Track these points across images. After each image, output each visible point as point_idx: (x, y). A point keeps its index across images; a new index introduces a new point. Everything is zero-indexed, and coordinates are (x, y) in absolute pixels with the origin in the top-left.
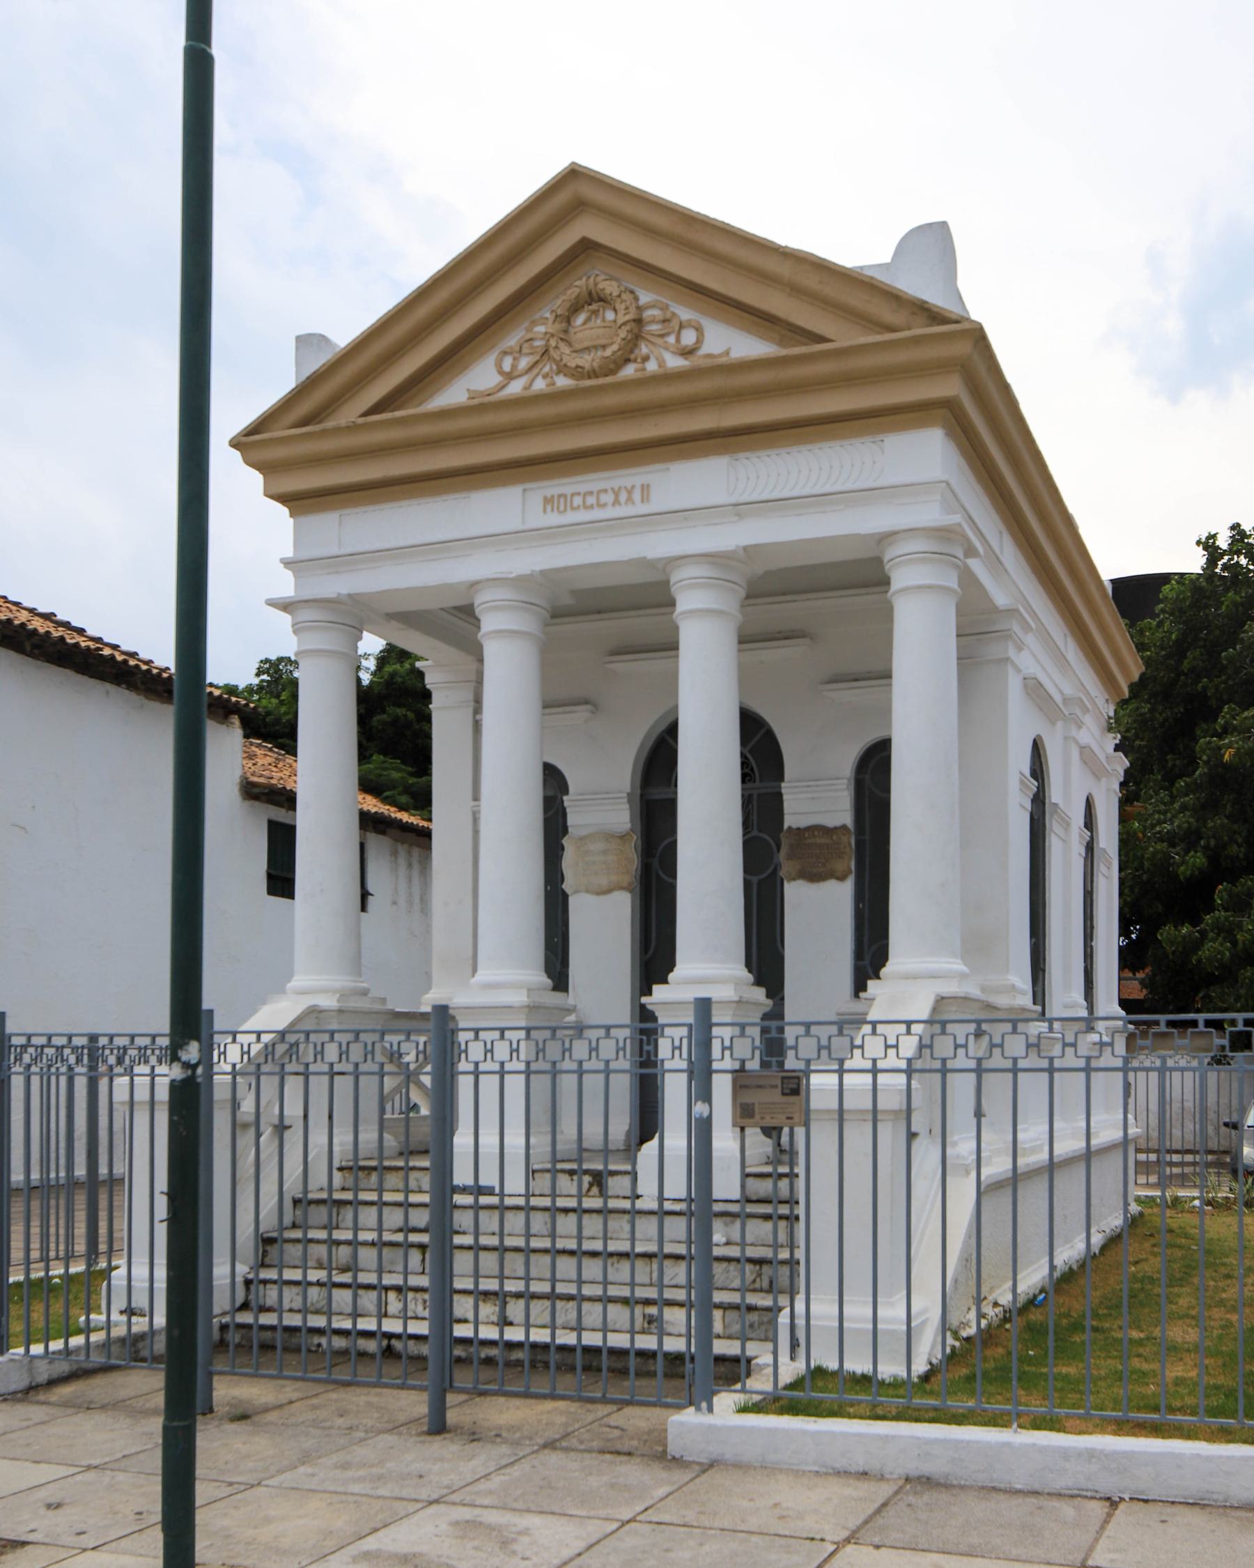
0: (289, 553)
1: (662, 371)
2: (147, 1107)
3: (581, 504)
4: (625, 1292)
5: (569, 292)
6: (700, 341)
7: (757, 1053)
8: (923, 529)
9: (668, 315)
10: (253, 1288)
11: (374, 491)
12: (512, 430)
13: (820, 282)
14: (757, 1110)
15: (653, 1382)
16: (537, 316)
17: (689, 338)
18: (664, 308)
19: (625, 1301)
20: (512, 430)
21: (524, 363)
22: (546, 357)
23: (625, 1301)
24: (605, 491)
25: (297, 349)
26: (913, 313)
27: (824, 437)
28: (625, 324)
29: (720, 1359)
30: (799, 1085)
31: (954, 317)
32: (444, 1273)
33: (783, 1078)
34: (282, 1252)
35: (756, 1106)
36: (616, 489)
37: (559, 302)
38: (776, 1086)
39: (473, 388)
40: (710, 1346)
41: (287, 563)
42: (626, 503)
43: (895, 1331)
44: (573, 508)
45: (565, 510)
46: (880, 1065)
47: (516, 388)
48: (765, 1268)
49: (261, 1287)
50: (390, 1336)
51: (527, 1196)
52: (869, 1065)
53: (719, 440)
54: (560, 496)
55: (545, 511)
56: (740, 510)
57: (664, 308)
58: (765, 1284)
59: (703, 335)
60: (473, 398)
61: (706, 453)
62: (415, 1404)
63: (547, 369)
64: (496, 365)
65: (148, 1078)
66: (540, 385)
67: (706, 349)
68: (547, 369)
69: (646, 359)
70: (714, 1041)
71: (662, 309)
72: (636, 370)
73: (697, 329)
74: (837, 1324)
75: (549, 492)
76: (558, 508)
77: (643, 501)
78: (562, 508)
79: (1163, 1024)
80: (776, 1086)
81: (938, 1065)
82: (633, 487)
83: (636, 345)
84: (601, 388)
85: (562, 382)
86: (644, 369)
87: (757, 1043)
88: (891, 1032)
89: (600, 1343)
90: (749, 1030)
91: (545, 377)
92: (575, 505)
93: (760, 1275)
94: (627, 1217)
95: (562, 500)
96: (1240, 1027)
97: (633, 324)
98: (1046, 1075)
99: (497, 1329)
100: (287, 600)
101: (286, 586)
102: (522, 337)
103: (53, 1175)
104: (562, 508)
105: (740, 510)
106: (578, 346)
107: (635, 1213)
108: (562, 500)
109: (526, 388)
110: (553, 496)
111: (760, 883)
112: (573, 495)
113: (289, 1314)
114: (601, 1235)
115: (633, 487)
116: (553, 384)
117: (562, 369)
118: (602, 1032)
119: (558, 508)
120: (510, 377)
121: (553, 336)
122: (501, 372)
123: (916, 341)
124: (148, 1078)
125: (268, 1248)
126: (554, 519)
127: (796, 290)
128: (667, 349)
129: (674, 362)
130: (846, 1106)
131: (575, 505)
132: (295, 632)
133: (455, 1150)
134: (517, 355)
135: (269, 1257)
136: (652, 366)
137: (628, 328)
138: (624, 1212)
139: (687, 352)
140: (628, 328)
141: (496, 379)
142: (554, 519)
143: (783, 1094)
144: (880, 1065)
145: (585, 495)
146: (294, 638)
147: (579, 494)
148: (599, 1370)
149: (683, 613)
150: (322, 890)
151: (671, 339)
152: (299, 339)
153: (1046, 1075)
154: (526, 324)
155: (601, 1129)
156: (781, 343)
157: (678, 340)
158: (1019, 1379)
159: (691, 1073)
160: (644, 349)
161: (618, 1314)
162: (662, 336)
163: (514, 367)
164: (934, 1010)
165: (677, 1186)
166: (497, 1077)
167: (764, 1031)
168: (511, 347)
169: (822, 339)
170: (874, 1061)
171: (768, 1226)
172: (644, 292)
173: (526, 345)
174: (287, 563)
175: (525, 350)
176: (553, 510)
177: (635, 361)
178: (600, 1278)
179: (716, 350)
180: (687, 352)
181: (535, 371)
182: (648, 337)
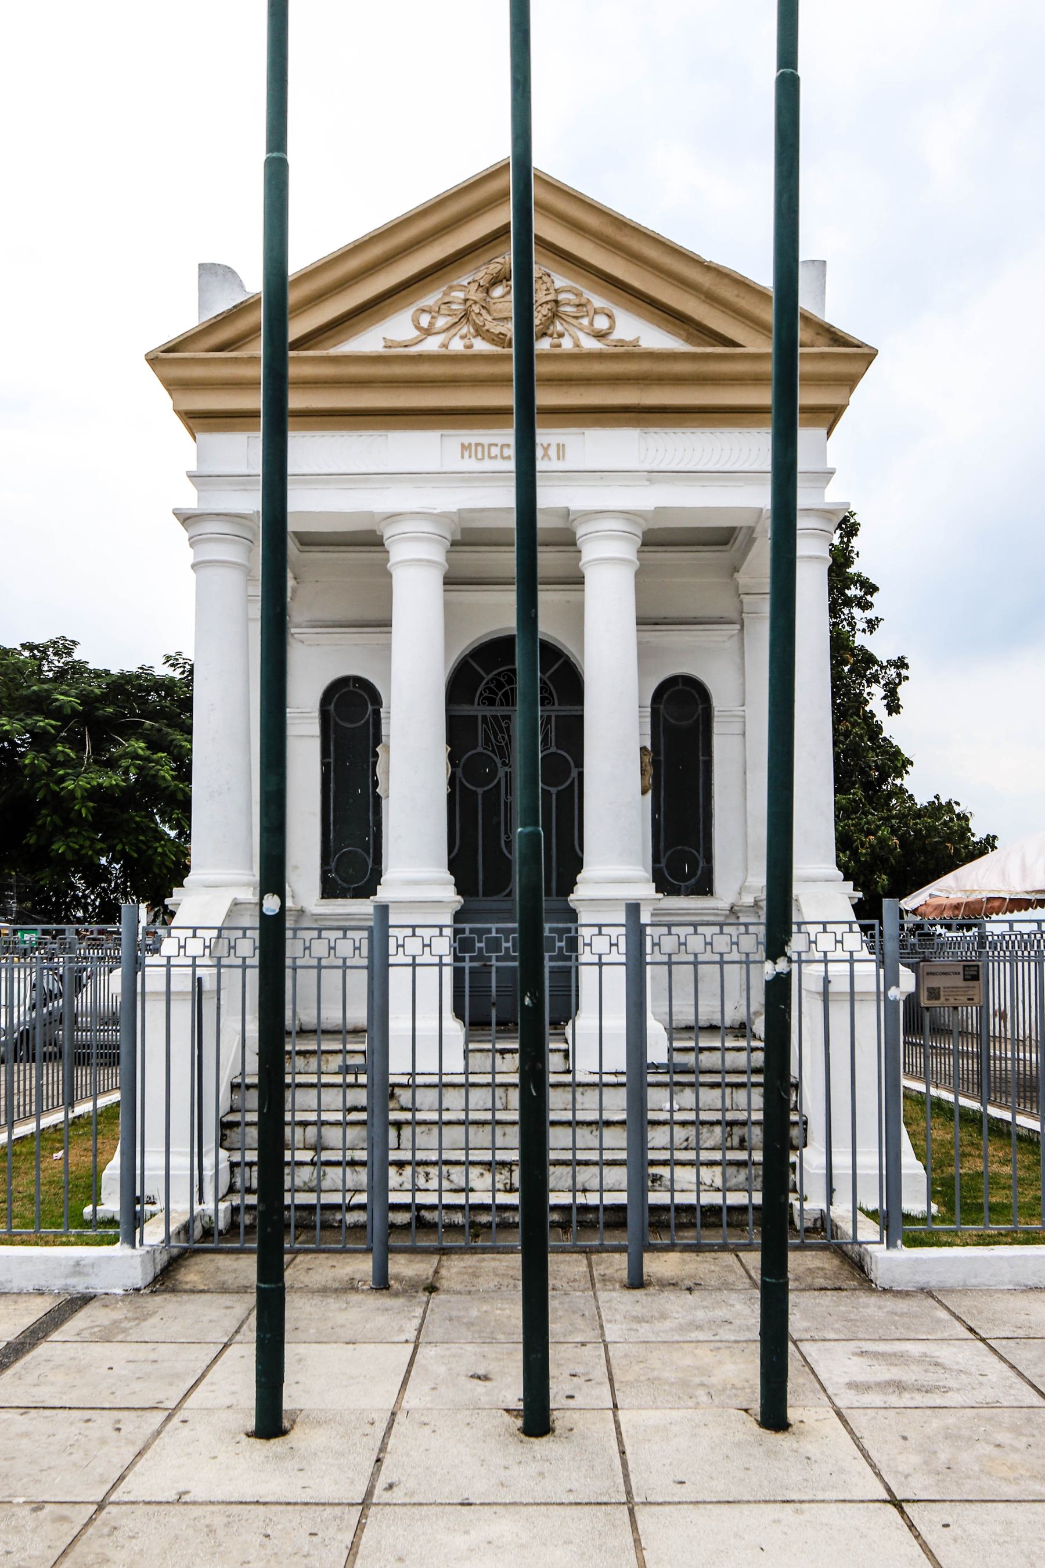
0: (193, 467)
1: (576, 350)
2: (164, 998)
3: (498, 453)
4: (487, 1156)
5: (492, 266)
6: (612, 327)
7: (257, 951)
8: (818, 510)
9: (583, 301)
10: (237, 1170)
11: (319, 419)
12: (442, 381)
13: (737, 296)
14: (942, 994)
15: (721, 1231)
16: (455, 283)
17: (601, 323)
18: (578, 294)
19: (488, 1165)
20: (442, 381)
21: (441, 322)
22: (464, 320)
23: (488, 1165)
24: (496, 445)
25: (200, 276)
26: (818, 334)
27: (703, 424)
28: (547, 303)
29: (656, 1209)
30: (978, 971)
31: (856, 342)
32: (639, 1144)
33: (965, 966)
34: (244, 1135)
35: (942, 990)
36: (545, 445)
37: (481, 274)
38: (959, 973)
39: (388, 337)
40: (644, 1197)
41: (191, 476)
42: (542, 458)
43: (916, 1174)
44: (490, 457)
45: (483, 458)
46: (418, 961)
47: (432, 345)
48: (735, 1129)
49: (247, 1169)
50: (421, 1207)
51: (466, 1073)
52: (315, 962)
53: (633, 415)
54: (477, 445)
55: (462, 457)
56: (654, 475)
57: (578, 294)
58: (736, 1142)
59: (614, 322)
60: (390, 347)
61: (619, 424)
62: (618, 1264)
63: (464, 331)
64: (413, 321)
65: (164, 969)
66: (457, 346)
67: (616, 335)
68: (464, 331)
69: (561, 335)
70: (390, 939)
71: (576, 295)
72: (553, 346)
73: (609, 316)
74: (851, 1172)
75: (467, 441)
76: (476, 455)
77: (559, 458)
78: (480, 455)
79: (494, 931)
80: (959, 973)
81: (847, 956)
82: (549, 445)
83: (553, 322)
84: (226, 360)
85: (481, 346)
86: (559, 346)
87: (257, 944)
88: (813, 929)
89: (315, 1202)
90: (249, 933)
91: (462, 337)
92: (493, 454)
93: (731, 1135)
94: (570, 1089)
95: (480, 449)
96: (467, 934)
97: (553, 304)
98: (437, 968)
99: (746, 1194)
100: (191, 511)
101: (190, 499)
102: (439, 300)
103: (22, 1068)
104: (480, 455)
105: (654, 475)
106: (496, 315)
107: (575, 1085)
108: (480, 449)
109: (445, 346)
110: (470, 444)
111: (559, 793)
112: (490, 445)
113: (449, 1194)
114: (570, 1106)
115: (549, 445)
116: (470, 346)
117: (480, 332)
118: (190, 932)
119: (476, 455)
120: (428, 332)
121: (475, 302)
122: (418, 327)
123: (823, 356)
124: (164, 969)
125: (228, 1132)
126: (470, 464)
127: (711, 298)
128: (581, 330)
129: (590, 344)
130: (857, 989)
131: (493, 454)
132: (191, 545)
133: (648, 1032)
134: (436, 315)
135: (228, 1140)
136: (567, 344)
137: (549, 306)
138: (312, 1086)
139: (600, 336)
140: (549, 306)
141: (413, 333)
142: (470, 464)
143: (965, 980)
144: (418, 961)
145: (502, 446)
146: (191, 551)
147: (496, 445)
148: (721, 1226)
149: (393, 565)
150: (229, 789)
151: (585, 321)
152: (202, 266)
153: (597, 967)
154: (444, 288)
155: (341, 1015)
156: (688, 339)
157: (591, 323)
158: (962, 1211)
159: (370, 968)
160: (559, 327)
161: (711, 1176)
162: (577, 318)
163: (431, 324)
164: (229, 915)
165: (617, 1059)
166: (240, 970)
167: (457, 932)
168: (431, 307)
169: (735, 344)
170: (851, 953)
171: (717, 1092)
172: (558, 276)
173: (443, 307)
174: (191, 476)
175: (442, 312)
176: (470, 457)
177: (551, 336)
178: (598, 1146)
179: (629, 337)
180: (600, 336)
181: (453, 331)
182: (564, 317)
